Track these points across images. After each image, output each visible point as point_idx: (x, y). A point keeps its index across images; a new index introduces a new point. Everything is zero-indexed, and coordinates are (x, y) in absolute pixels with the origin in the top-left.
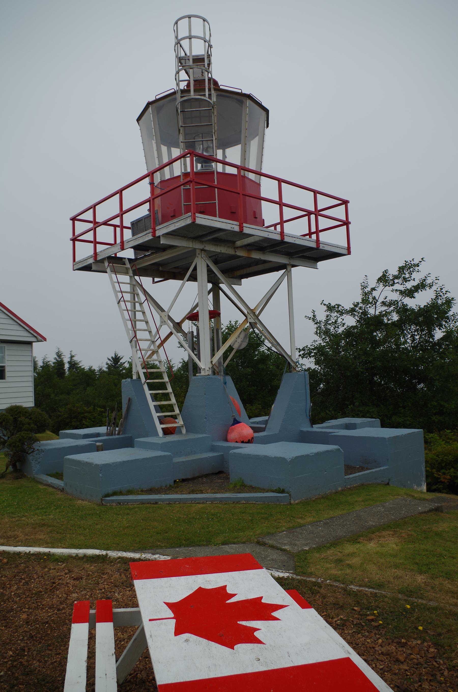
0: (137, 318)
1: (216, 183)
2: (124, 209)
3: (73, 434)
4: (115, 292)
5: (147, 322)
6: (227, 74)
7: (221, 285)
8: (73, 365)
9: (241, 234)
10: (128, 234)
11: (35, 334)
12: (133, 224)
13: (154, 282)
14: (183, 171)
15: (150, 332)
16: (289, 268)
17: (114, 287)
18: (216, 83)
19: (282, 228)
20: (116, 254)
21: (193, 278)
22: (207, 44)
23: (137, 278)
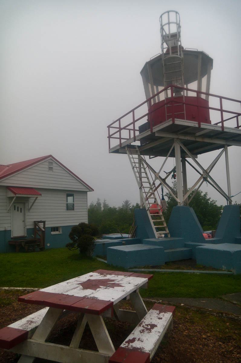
0: (142, 176)
1: (184, 101)
2: (135, 119)
3: (109, 237)
4: (131, 163)
5: (148, 178)
6: (188, 43)
7: (187, 159)
8: (105, 205)
9: (199, 129)
10: (137, 133)
11: (88, 187)
12: (140, 127)
13: (150, 158)
14: (166, 97)
15: (150, 183)
16: (226, 146)
17: (130, 161)
18: (183, 48)
19: (223, 124)
20: (130, 144)
21: (173, 155)
22: (178, 26)
23: (142, 156)
